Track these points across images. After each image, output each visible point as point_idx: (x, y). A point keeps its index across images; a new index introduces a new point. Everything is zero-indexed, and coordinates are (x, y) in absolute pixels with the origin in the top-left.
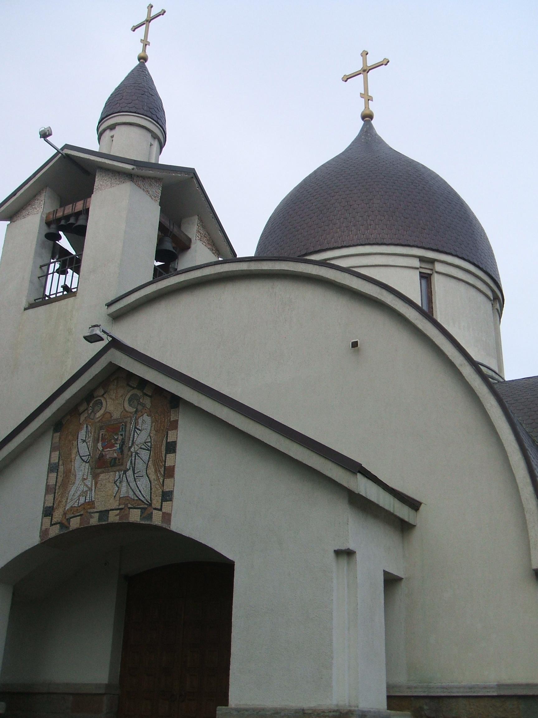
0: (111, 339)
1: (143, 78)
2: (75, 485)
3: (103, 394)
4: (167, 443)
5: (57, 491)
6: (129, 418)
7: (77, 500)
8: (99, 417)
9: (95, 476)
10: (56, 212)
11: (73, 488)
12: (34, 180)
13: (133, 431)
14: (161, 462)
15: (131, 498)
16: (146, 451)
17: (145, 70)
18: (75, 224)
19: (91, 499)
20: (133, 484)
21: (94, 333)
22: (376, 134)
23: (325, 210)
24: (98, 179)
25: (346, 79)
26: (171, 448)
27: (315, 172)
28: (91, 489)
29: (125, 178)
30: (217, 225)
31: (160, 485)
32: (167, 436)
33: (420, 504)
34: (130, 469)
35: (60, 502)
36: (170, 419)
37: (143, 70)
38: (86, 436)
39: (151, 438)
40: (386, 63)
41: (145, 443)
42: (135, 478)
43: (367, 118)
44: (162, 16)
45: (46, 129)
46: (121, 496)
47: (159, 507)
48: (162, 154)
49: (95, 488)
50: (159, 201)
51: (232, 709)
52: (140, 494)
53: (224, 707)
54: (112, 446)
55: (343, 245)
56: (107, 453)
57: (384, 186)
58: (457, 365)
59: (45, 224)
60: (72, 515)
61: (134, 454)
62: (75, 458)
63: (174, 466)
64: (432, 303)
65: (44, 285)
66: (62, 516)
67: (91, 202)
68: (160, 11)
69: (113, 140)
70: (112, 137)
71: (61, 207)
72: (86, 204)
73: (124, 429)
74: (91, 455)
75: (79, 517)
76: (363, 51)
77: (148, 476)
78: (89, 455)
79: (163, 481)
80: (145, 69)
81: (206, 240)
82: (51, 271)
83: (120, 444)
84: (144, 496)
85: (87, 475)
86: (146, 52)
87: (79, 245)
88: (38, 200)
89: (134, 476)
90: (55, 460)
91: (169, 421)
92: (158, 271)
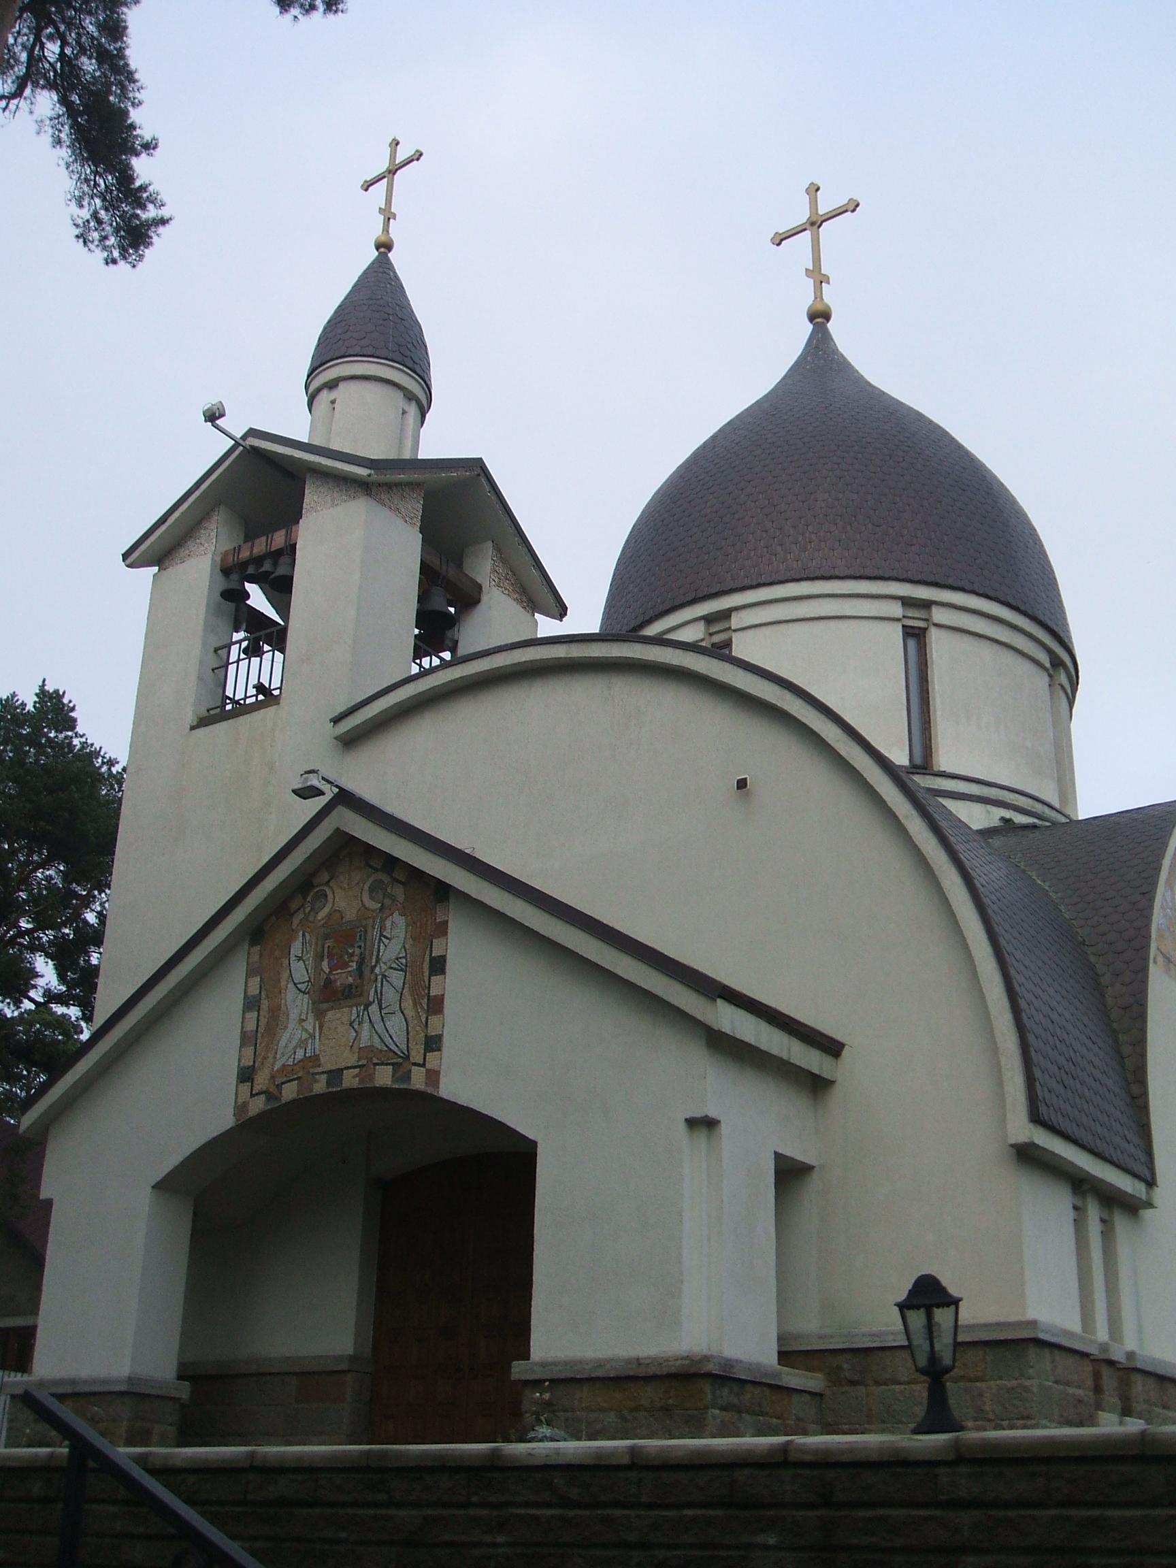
0: (338, 790)
1: (386, 287)
2: (287, 1030)
3: (329, 881)
4: (432, 959)
5: (258, 1041)
6: (371, 920)
7: (291, 1056)
8: (323, 919)
9: (320, 1015)
10: (239, 552)
11: (284, 1035)
12: (197, 493)
13: (377, 941)
14: (424, 990)
15: (377, 1049)
16: (399, 972)
17: (389, 269)
18: (273, 573)
19: (314, 1052)
20: (379, 1027)
21: (309, 784)
22: (835, 351)
23: (728, 516)
24: (309, 491)
25: (779, 240)
26: (438, 966)
27: (714, 438)
28: (312, 1036)
29: (357, 489)
30: (528, 558)
31: (422, 1026)
32: (431, 948)
33: (841, 1046)
34: (374, 1001)
35: (265, 1058)
36: (435, 919)
37: (385, 270)
38: (303, 951)
39: (405, 951)
40: (852, 208)
41: (397, 959)
42: (381, 1016)
43: (819, 317)
44: (415, 162)
45: (214, 405)
46: (361, 1046)
47: (421, 1062)
48: (425, 425)
49: (320, 1034)
50: (419, 524)
51: (536, 1364)
52: (391, 1041)
53: (523, 1362)
54: (346, 965)
55: (760, 581)
56: (337, 977)
57: (836, 466)
58: (901, 818)
59: (220, 572)
60: (285, 1079)
61: (380, 977)
62: (287, 987)
63: (443, 995)
64: (927, 681)
65: (223, 683)
66: (269, 1080)
67: (300, 533)
68: (413, 153)
69: (334, 408)
70: (333, 402)
71: (245, 541)
72: (291, 536)
73: (363, 938)
74: (312, 981)
75: (296, 1082)
76: (810, 184)
77: (402, 1012)
78: (308, 982)
79: (427, 1019)
80: (388, 266)
81: (508, 584)
82: (233, 657)
83: (357, 962)
84: (398, 1044)
85: (307, 1014)
86: (390, 232)
87: (283, 607)
88: (206, 528)
89: (381, 1012)
90: (254, 990)
91: (433, 924)
92: (422, 651)
